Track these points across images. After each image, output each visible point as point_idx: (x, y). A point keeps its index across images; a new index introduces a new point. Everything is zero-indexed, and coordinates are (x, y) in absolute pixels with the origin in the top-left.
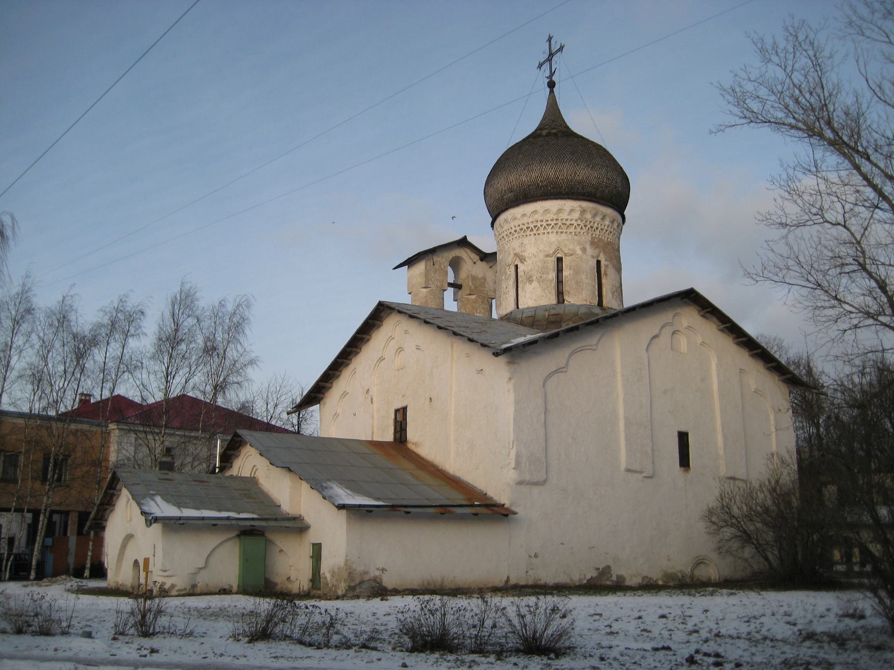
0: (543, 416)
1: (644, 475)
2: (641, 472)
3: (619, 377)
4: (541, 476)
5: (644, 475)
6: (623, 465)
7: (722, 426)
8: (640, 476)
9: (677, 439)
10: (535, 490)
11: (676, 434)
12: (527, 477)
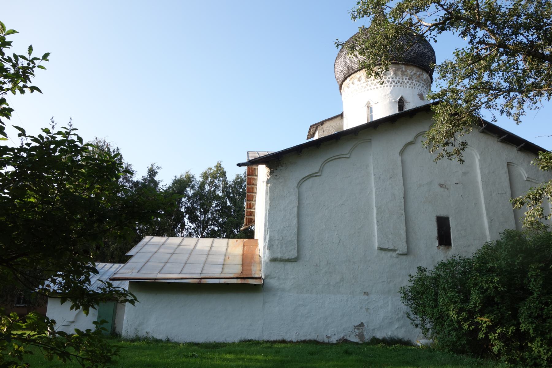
0: (296, 209)
1: (397, 252)
2: (395, 251)
3: (373, 176)
4: (293, 254)
5: (397, 252)
6: (376, 245)
7: (487, 210)
8: (394, 254)
9: (435, 224)
10: (289, 266)
11: (434, 219)
12: (279, 255)
